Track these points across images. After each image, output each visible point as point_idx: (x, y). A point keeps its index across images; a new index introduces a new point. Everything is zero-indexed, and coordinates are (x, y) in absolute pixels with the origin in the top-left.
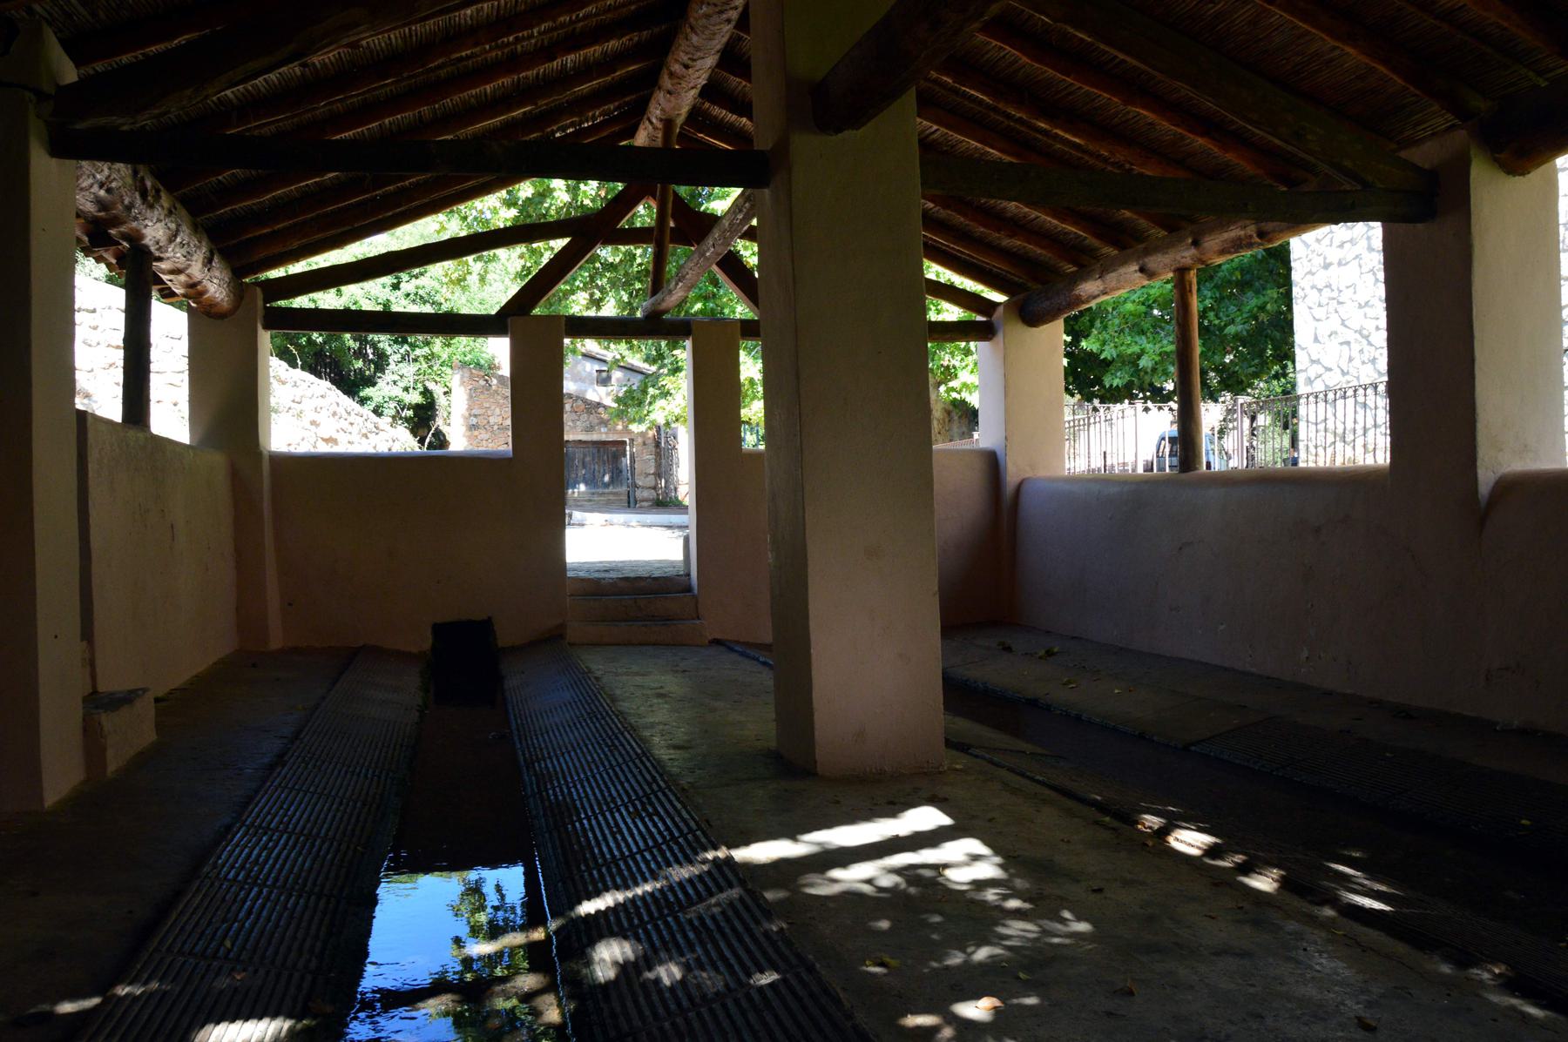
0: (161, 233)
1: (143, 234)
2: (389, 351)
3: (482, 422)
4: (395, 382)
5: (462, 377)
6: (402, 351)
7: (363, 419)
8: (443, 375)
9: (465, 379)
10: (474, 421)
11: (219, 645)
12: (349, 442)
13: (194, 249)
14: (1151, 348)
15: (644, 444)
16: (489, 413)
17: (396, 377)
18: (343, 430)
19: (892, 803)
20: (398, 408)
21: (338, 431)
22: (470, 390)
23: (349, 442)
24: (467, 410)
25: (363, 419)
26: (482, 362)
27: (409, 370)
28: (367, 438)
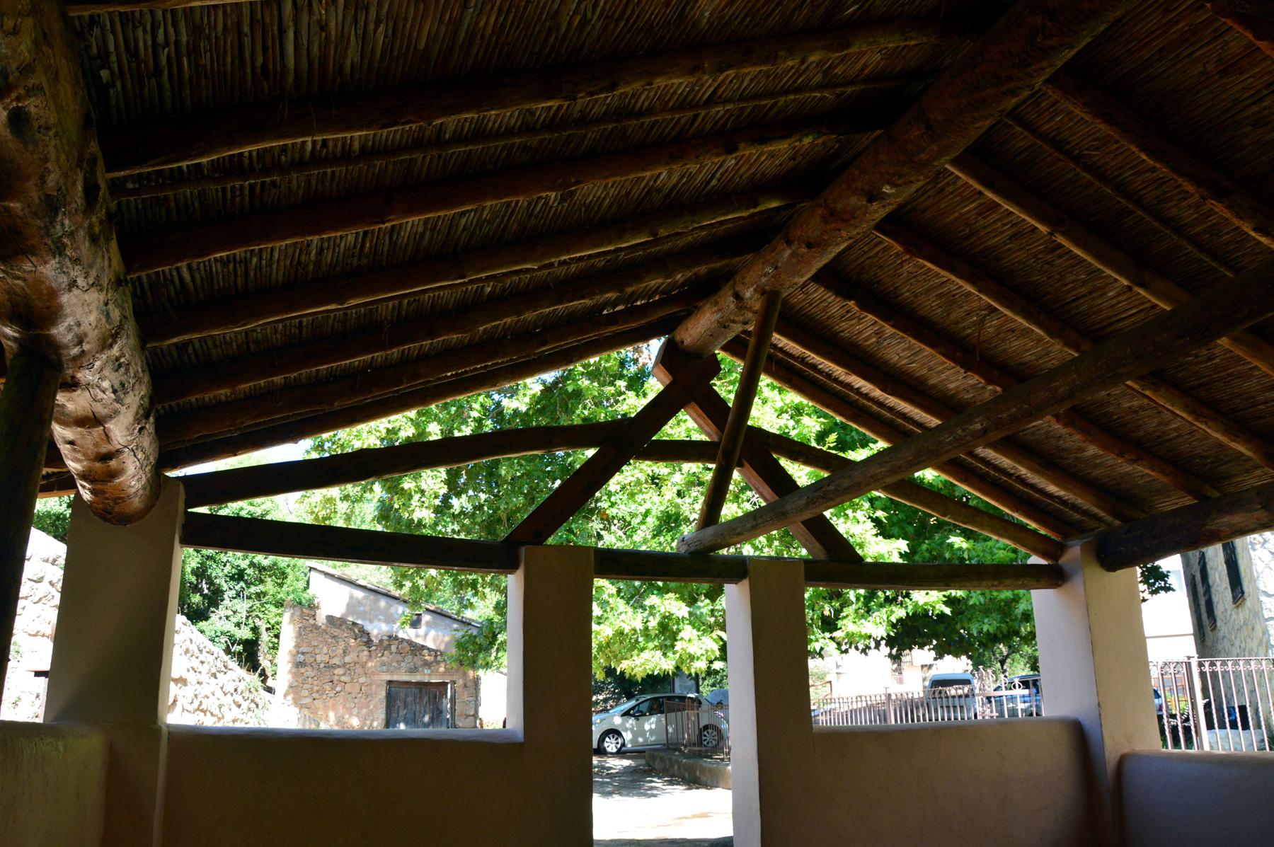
0: (92, 318)
1: (60, 308)
2: (225, 587)
3: (309, 659)
4: (227, 617)
5: (293, 615)
6: (237, 588)
7: (213, 657)
8: (266, 612)
9: (296, 618)
10: (301, 658)
12: (198, 683)
13: (132, 381)
15: (465, 686)
16: (317, 651)
17: (230, 613)
18: (193, 669)
20: (229, 643)
21: (189, 671)
22: (300, 628)
23: (198, 683)
24: (295, 646)
25: (213, 657)
26: (304, 601)
27: (242, 606)
28: (216, 678)
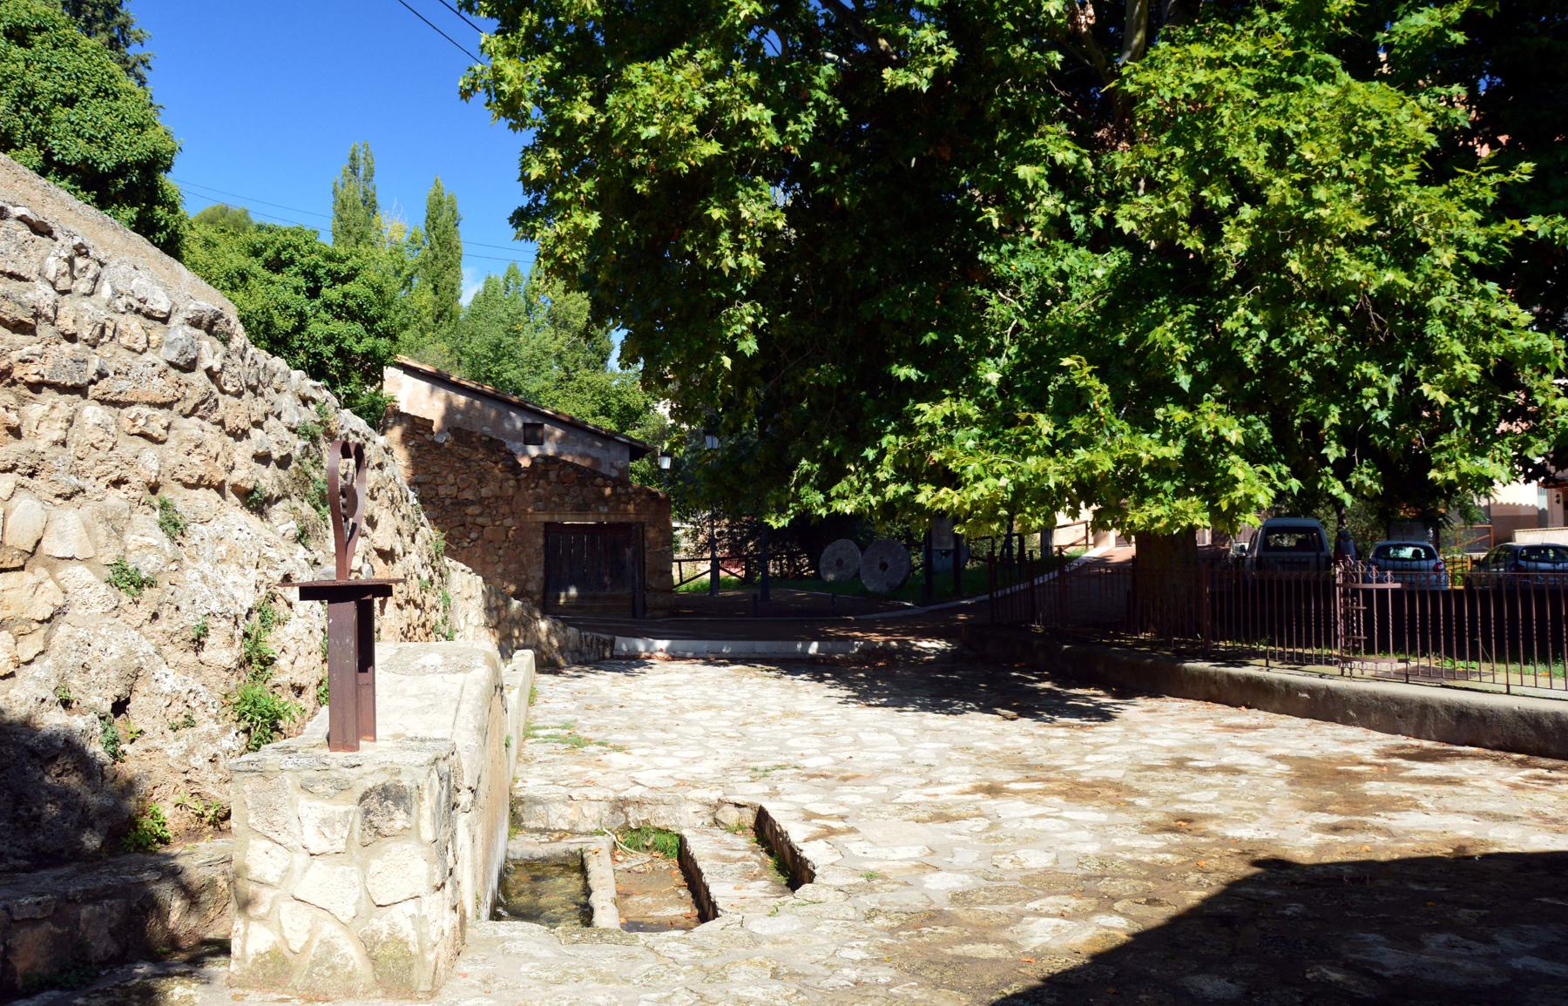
11: (196, 885)
14: (943, 53)
16: (439, 480)
19: (1227, 921)
